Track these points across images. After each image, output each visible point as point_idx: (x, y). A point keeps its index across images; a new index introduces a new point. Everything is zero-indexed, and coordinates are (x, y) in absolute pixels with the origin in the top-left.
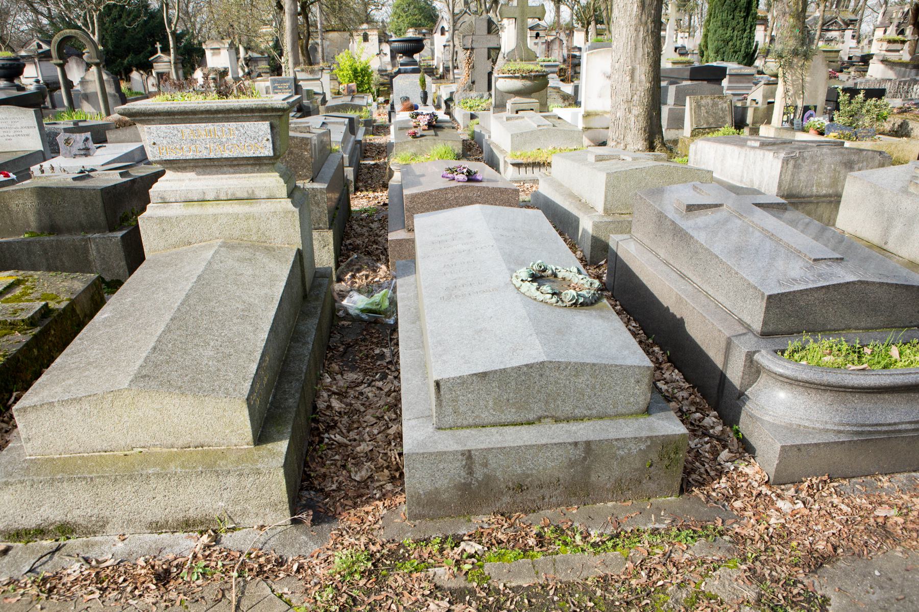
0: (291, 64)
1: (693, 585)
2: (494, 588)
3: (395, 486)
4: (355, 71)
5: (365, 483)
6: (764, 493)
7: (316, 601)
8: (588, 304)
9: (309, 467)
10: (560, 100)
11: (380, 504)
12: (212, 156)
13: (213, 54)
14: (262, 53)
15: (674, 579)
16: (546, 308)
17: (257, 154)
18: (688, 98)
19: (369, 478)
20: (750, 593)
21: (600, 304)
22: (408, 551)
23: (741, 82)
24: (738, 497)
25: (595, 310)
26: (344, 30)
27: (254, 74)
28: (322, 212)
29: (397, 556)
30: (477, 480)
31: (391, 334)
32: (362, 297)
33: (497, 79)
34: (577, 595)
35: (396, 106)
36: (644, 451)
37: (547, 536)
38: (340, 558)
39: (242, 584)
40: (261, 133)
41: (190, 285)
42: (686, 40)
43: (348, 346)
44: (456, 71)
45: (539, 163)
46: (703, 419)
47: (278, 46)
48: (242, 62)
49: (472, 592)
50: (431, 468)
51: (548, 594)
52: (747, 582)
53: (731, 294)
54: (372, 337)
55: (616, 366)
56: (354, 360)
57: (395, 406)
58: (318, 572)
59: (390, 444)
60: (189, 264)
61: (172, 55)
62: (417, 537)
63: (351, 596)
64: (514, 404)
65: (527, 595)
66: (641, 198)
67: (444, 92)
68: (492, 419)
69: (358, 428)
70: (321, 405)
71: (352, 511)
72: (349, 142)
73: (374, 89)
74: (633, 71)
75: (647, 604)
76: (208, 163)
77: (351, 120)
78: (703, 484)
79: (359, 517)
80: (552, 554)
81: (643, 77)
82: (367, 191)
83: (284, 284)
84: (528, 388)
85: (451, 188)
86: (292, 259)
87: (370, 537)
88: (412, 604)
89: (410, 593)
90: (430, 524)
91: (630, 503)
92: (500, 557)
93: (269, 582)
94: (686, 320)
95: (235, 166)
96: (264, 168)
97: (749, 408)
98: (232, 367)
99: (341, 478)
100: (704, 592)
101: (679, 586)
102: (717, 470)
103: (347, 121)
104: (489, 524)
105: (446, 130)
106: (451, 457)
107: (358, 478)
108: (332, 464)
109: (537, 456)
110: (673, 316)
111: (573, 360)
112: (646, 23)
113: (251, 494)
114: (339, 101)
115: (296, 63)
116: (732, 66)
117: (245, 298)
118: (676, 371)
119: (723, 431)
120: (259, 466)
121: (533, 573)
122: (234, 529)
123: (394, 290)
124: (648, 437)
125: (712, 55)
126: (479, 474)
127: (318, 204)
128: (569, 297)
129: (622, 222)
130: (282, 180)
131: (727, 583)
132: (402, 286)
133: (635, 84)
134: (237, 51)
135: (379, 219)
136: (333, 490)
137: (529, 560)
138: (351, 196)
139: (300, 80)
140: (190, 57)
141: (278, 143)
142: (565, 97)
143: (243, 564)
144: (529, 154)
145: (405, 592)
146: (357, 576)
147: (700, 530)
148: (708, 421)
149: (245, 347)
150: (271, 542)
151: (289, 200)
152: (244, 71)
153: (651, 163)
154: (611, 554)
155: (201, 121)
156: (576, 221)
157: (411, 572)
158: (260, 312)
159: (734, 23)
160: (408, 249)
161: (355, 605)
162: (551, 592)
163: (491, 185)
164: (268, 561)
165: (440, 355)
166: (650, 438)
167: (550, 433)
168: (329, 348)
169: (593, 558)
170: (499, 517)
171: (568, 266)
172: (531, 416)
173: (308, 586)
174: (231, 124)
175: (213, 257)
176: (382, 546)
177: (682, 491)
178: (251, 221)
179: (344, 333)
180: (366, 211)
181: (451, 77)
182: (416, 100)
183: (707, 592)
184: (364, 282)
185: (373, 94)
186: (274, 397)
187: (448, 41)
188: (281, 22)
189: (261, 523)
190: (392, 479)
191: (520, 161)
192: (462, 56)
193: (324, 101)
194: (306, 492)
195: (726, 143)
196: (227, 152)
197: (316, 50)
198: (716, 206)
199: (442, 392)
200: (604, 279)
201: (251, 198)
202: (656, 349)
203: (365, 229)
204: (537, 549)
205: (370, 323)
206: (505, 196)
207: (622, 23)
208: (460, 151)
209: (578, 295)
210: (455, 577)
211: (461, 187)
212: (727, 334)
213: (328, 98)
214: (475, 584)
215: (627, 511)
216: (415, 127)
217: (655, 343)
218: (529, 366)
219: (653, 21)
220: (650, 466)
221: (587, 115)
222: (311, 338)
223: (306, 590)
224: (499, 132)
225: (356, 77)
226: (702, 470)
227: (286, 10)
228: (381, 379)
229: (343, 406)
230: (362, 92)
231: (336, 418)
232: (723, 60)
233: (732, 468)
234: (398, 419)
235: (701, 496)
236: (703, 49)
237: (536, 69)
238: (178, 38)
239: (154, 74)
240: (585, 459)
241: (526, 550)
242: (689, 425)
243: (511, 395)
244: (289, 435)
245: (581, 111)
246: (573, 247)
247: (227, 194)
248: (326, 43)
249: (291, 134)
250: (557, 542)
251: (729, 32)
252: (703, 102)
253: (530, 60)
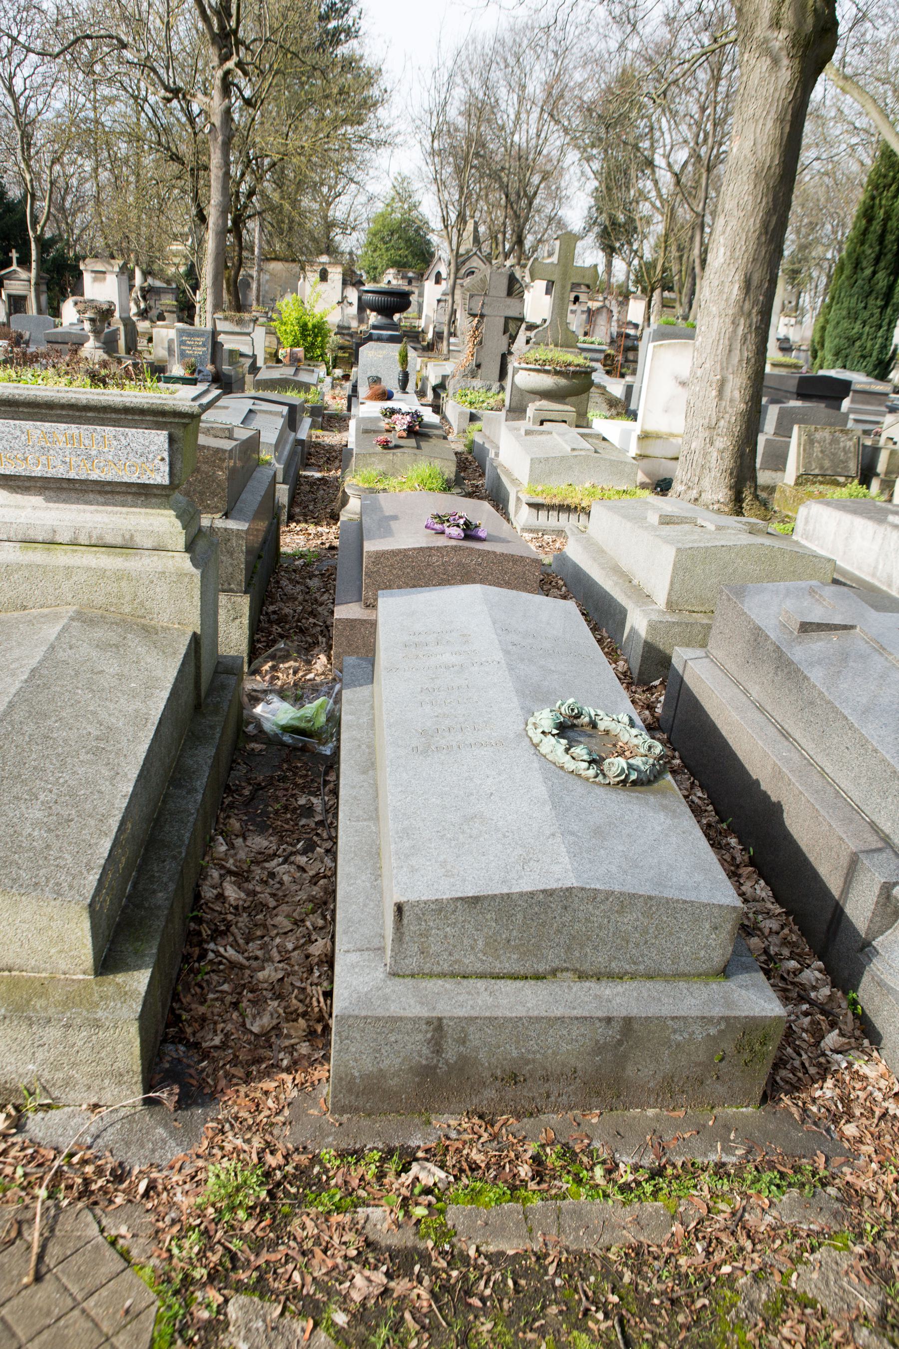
0: (209, 306)
1: (777, 1277)
2: (461, 1252)
3: (314, 1048)
4: (304, 327)
5: (266, 1038)
6: (891, 1112)
7: (171, 1257)
8: (639, 783)
9: (179, 1000)
10: (605, 406)
11: (288, 1078)
12: (72, 475)
13: (95, 280)
14: (168, 282)
15: (748, 1262)
16: (579, 788)
17: (144, 480)
18: (796, 428)
19: (273, 1028)
20: (869, 1304)
21: (662, 783)
22: (326, 1171)
23: (868, 403)
24: (851, 1117)
25: (655, 793)
26: (294, 261)
27: (154, 313)
28: (235, 564)
29: (308, 1179)
30: (447, 1063)
31: (326, 773)
32: (286, 705)
33: (516, 370)
34: (592, 1279)
35: (360, 389)
36: (714, 1038)
37: (549, 1162)
38: (219, 1172)
39: (52, 1212)
40: (153, 448)
41: (18, 685)
42: (792, 329)
43: (259, 787)
44: (452, 340)
45: (568, 507)
46: (801, 971)
47: (192, 275)
48: (136, 293)
49: (425, 1258)
50: (375, 1040)
51: (546, 1273)
52: (864, 1278)
53: (863, 780)
54: (295, 774)
55: (685, 902)
56: (265, 813)
57: (325, 903)
58: (179, 1198)
59: (311, 971)
60: (19, 644)
61: (34, 272)
62: (343, 1146)
63: (230, 1251)
64: (516, 947)
65: (513, 1272)
66: (729, 599)
67: (433, 373)
68: (479, 967)
69: (263, 937)
70: (208, 893)
71: (243, 1089)
72: (286, 442)
73: (329, 357)
74: (722, 384)
75: (704, 1306)
76: (65, 485)
77: (293, 409)
78: (798, 1089)
79: (253, 1100)
80: (556, 1197)
81: (737, 394)
82: (306, 522)
83: (166, 694)
84: (543, 924)
85: (438, 549)
86: (183, 650)
87: (268, 1137)
88: (326, 1274)
89: (325, 1252)
90: (365, 1122)
91: (680, 1113)
92: (475, 1196)
93: (98, 1211)
94: (785, 808)
95: (107, 493)
96: (154, 500)
97: (877, 967)
98: (70, 844)
99: (229, 1027)
100: (794, 1291)
101: (757, 1278)
102: (820, 1065)
103: (285, 410)
104: (459, 1133)
105: (434, 441)
106: (410, 1026)
107: (256, 1029)
108: (217, 999)
109: (546, 1033)
110: (765, 796)
111: (617, 888)
112: (750, 314)
113: (82, 1056)
114: (276, 374)
115: (218, 306)
116: (859, 379)
117: (103, 715)
118: (762, 882)
119: (831, 998)
120: (100, 1014)
121: (524, 1231)
122: (49, 1107)
123: (338, 700)
124: (722, 1018)
125: (829, 357)
126: (451, 1053)
127: (231, 554)
128: (615, 770)
129: (692, 624)
130: (178, 524)
131: (832, 1277)
132: (350, 702)
133: (724, 403)
134: (132, 277)
135: (323, 575)
136: (216, 1047)
137: (519, 1206)
138: (283, 528)
139: (220, 333)
140: (61, 278)
141: (178, 465)
142: (612, 403)
143: (59, 1173)
144: (555, 491)
145: (317, 1250)
146: (241, 1214)
147: (790, 1172)
148: (811, 975)
149: (95, 808)
150: (108, 1136)
151: (187, 555)
152: (138, 306)
153: (745, 539)
154: (650, 1205)
155: (59, 419)
156: (623, 613)
157: (329, 1212)
158: (124, 743)
159: (866, 314)
160: (364, 638)
161: (234, 1268)
162: (552, 1270)
163: (498, 548)
164: (100, 1172)
165: (407, 856)
166: (726, 1019)
167: (570, 998)
168: (228, 790)
169: (621, 1211)
170: (476, 1120)
171: (619, 716)
172: (542, 968)
173: (161, 1224)
174: (108, 429)
175: (58, 638)
176: (286, 1157)
177: (764, 1099)
178: (124, 584)
179: (253, 764)
180: (302, 556)
181: (445, 351)
182: (391, 383)
183: (800, 1291)
184: (291, 679)
185: (327, 363)
186: (134, 886)
187: (444, 294)
188: (201, 242)
189: (94, 1100)
190: (311, 1035)
191: (540, 500)
192: (463, 322)
193: (254, 369)
194: (171, 1047)
195: (854, 512)
196: (97, 471)
197: (248, 286)
198: (845, 627)
199: (405, 921)
200: (659, 710)
201: (127, 547)
202: (733, 841)
203: (299, 588)
204: (532, 1185)
205: (295, 749)
207: (714, 309)
208: (452, 476)
209: (630, 767)
210: (399, 1226)
211: (454, 548)
212: (853, 846)
213: (260, 363)
214: (430, 1244)
215: (677, 1127)
216: (388, 431)
217: (731, 830)
218: (549, 893)
219: (760, 312)
220: (721, 1061)
221: (645, 437)
222: (201, 782)
223: (157, 1232)
224: (513, 451)
225: (304, 336)
226: (797, 1063)
227: (211, 225)
228: (304, 852)
229: (243, 895)
230: (311, 358)
231: (230, 917)
232: (844, 367)
233: (844, 1065)
234: (328, 929)
235: (794, 1110)
236: (818, 347)
237: (576, 362)
238: (44, 245)
239: (4, 297)
240: (620, 1043)
241: (515, 1187)
242: (777, 981)
243: (515, 933)
244: (153, 960)
245: (635, 428)
246: (612, 653)
247: (90, 537)
248: (265, 277)
249: (202, 440)
250: (566, 1177)
251: (858, 326)
252: (818, 436)
253: (568, 346)
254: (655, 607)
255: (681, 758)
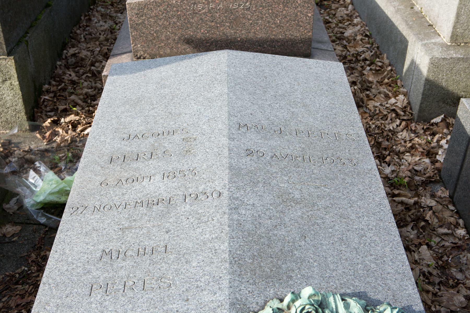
156: (401, 46)
200: (441, 157)
206: (291, 11)
254: (438, 40)
255: (466, 227)
